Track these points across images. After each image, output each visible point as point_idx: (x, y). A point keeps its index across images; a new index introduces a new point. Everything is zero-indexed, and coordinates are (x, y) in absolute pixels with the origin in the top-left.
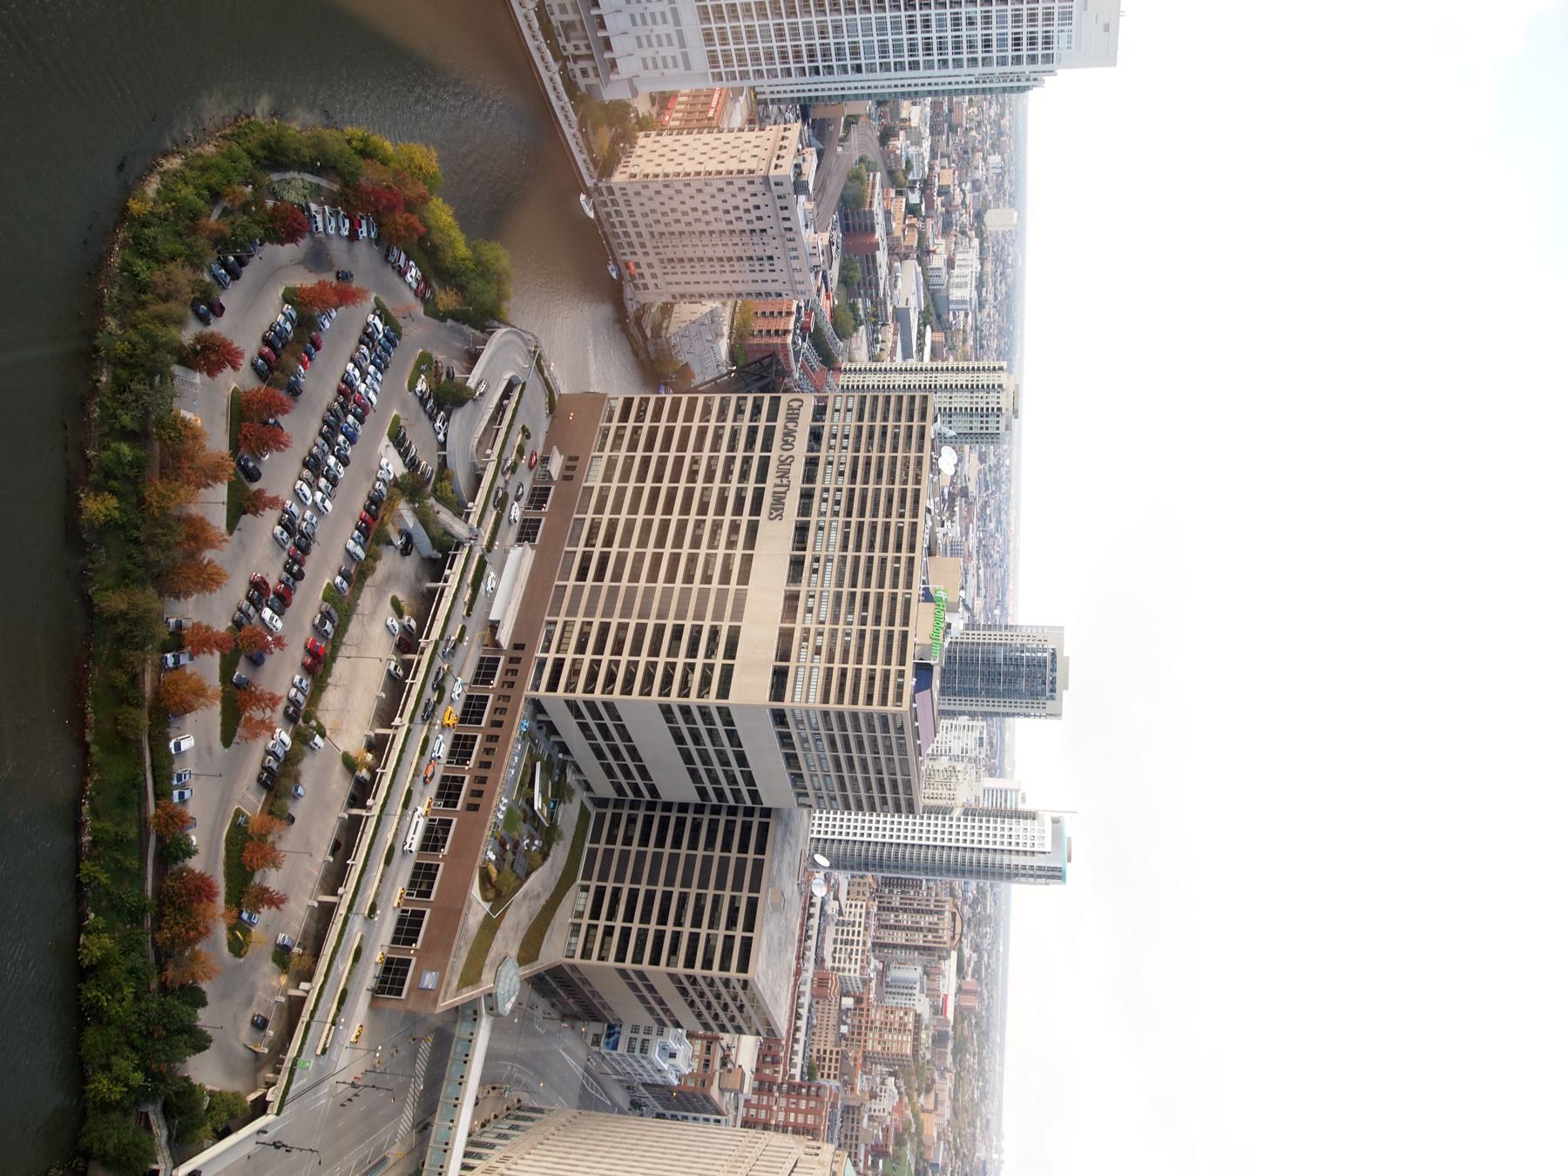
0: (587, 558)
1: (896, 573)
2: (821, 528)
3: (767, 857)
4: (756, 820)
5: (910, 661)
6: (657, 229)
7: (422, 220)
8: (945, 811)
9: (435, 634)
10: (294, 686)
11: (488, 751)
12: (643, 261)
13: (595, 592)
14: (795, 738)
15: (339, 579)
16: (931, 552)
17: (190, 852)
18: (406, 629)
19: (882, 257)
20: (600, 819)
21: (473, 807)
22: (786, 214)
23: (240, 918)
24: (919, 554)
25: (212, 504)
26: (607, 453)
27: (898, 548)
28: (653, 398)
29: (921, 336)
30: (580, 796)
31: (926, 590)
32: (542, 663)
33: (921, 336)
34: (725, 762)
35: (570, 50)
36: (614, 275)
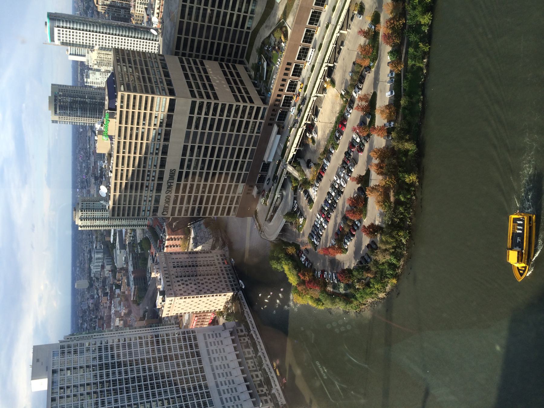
0: (245, 157)
1: (124, 148)
2: (155, 166)
3: (177, 35)
4: (181, 51)
5: (118, 112)
6: (217, 277)
7: (299, 277)
8: (102, 49)
9: (300, 130)
10: (350, 113)
11: (283, 85)
12: (222, 265)
13: (242, 144)
14: (165, 84)
15: (333, 152)
16: (110, 155)
17: (391, 53)
18: (311, 133)
19: (131, 269)
20: (242, 56)
21: (289, 64)
22: (168, 283)
23: (375, 27)
24: (115, 154)
25: (376, 179)
26: (236, 195)
27: (123, 157)
28: (219, 215)
29: (115, 239)
30: (249, 66)
31: (111, 140)
32: (262, 118)
33: (115, 239)
34: (193, 75)
35: (246, 339)
36: (232, 260)
